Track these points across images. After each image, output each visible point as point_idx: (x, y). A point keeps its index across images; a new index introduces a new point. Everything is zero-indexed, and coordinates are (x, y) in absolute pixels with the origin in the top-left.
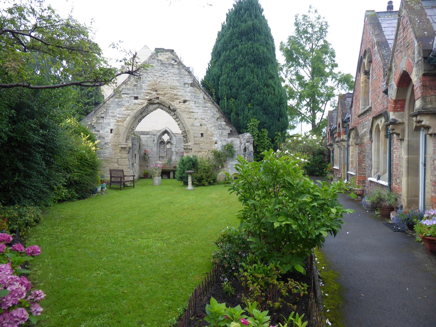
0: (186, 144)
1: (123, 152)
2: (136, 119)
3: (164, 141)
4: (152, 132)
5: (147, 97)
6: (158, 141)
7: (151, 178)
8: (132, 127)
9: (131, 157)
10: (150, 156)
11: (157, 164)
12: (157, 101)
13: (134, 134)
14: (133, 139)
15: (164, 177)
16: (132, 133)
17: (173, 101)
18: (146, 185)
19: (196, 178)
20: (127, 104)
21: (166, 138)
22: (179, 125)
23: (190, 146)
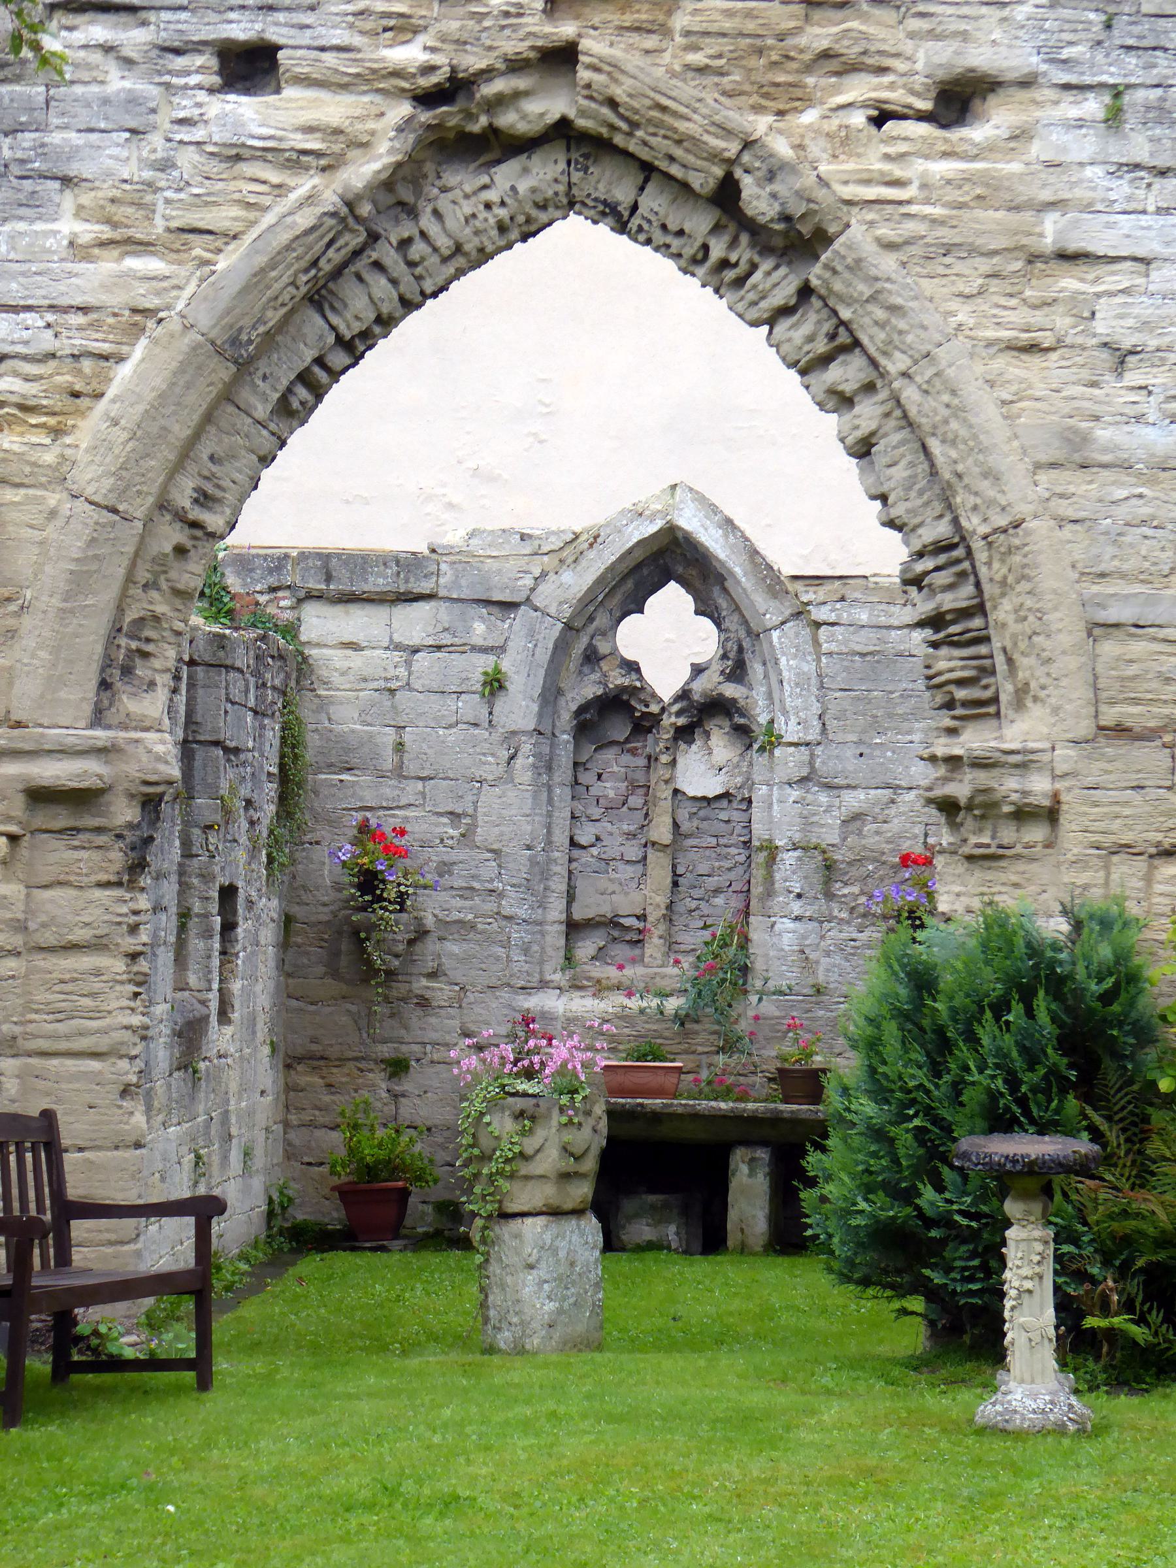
0: (976, 740)
1: (58, 855)
2: (244, 367)
3: (640, 691)
4: (462, 559)
5: (409, 54)
6: (551, 695)
7: (451, 1233)
8: (183, 498)
9: (168, 922)
10: (432, 907)
11: (536, 1021)
12: (547, 105)
13: (215, 600)
14: (202, 666)
15: (642, 1230)
16: (191, 575)
17: (786, 100)
18: (378, 1340)
19: (1117, 1250)
20: (114, 161)
21: (667, 643)
22: (863, 450)
23: (1024, 762)
